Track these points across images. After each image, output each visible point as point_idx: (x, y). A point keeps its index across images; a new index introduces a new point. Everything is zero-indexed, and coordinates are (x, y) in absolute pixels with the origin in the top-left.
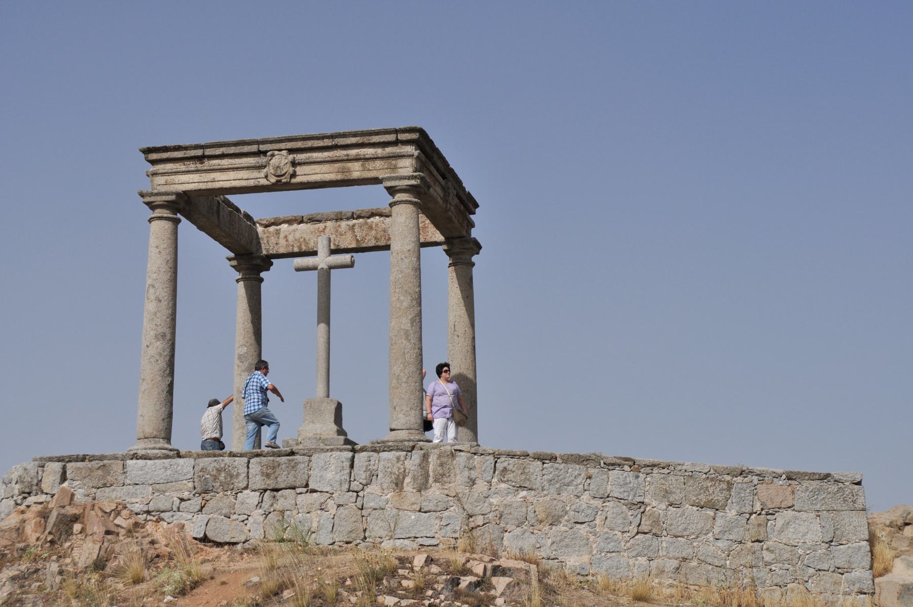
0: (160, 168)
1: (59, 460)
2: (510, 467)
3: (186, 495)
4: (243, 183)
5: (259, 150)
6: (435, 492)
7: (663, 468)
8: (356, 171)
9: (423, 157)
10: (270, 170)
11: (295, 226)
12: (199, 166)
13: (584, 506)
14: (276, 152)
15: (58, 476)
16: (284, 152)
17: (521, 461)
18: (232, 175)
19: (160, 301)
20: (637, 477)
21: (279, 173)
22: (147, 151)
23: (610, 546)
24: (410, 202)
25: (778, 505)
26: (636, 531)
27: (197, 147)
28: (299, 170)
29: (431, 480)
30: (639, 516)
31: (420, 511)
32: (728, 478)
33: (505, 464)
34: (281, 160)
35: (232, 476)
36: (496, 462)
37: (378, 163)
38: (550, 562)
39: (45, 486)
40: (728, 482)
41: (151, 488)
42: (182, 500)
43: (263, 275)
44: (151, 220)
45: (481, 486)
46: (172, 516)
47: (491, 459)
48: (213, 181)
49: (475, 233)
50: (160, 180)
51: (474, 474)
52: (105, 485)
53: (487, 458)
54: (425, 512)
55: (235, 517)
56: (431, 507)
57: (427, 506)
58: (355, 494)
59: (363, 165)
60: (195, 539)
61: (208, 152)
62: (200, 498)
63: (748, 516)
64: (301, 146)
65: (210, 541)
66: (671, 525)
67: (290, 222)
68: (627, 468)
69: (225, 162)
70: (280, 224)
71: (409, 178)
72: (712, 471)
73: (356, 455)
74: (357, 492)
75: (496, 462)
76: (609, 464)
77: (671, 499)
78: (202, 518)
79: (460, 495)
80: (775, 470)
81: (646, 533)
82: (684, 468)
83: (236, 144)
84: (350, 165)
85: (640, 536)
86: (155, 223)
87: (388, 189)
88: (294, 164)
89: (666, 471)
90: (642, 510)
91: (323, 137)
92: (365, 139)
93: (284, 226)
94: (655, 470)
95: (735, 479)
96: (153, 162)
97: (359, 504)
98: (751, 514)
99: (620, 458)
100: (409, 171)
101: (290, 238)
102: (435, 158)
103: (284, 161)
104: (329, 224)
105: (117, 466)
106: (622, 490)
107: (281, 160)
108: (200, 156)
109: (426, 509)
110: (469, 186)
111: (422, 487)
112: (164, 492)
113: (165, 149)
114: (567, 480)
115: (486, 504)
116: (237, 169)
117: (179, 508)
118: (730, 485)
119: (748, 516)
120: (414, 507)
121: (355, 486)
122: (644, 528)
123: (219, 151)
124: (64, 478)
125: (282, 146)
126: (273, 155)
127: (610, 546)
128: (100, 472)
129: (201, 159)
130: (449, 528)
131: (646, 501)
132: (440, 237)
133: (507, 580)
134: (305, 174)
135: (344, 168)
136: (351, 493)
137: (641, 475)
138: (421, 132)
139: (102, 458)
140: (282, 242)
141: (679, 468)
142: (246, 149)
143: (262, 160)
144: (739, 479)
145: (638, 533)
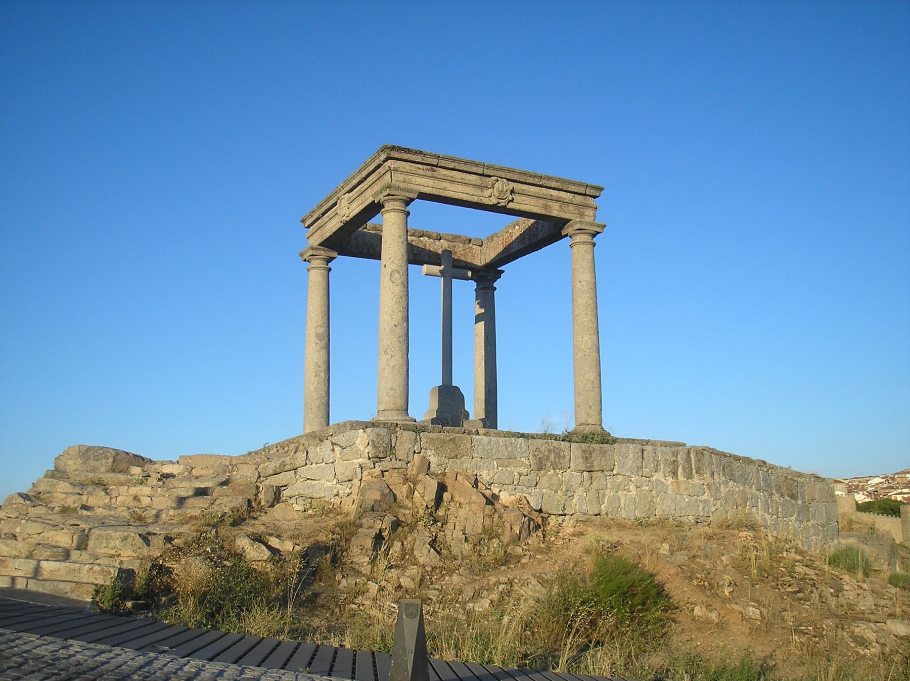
4: (469, 198)
6: (696, 480)
12: (429, 173)
18: (460, 188)
24: (583, 243)
28: (517, 198)
29: (694, 471)
35: (560, 457)
37: (571, 208)
42: (520, 475)
43: (440, 252)
48: (445, 189)
52: (456, 457)
59: (560, 206)
61: (442, 163)
83: (466, 163)
84: (550, 203)
113: (408, 151)
116: (365, 179)
123: (451, 165)
125: (503, 174)
128: (452, 445)
135: (546, 205)
142: (474, 169)
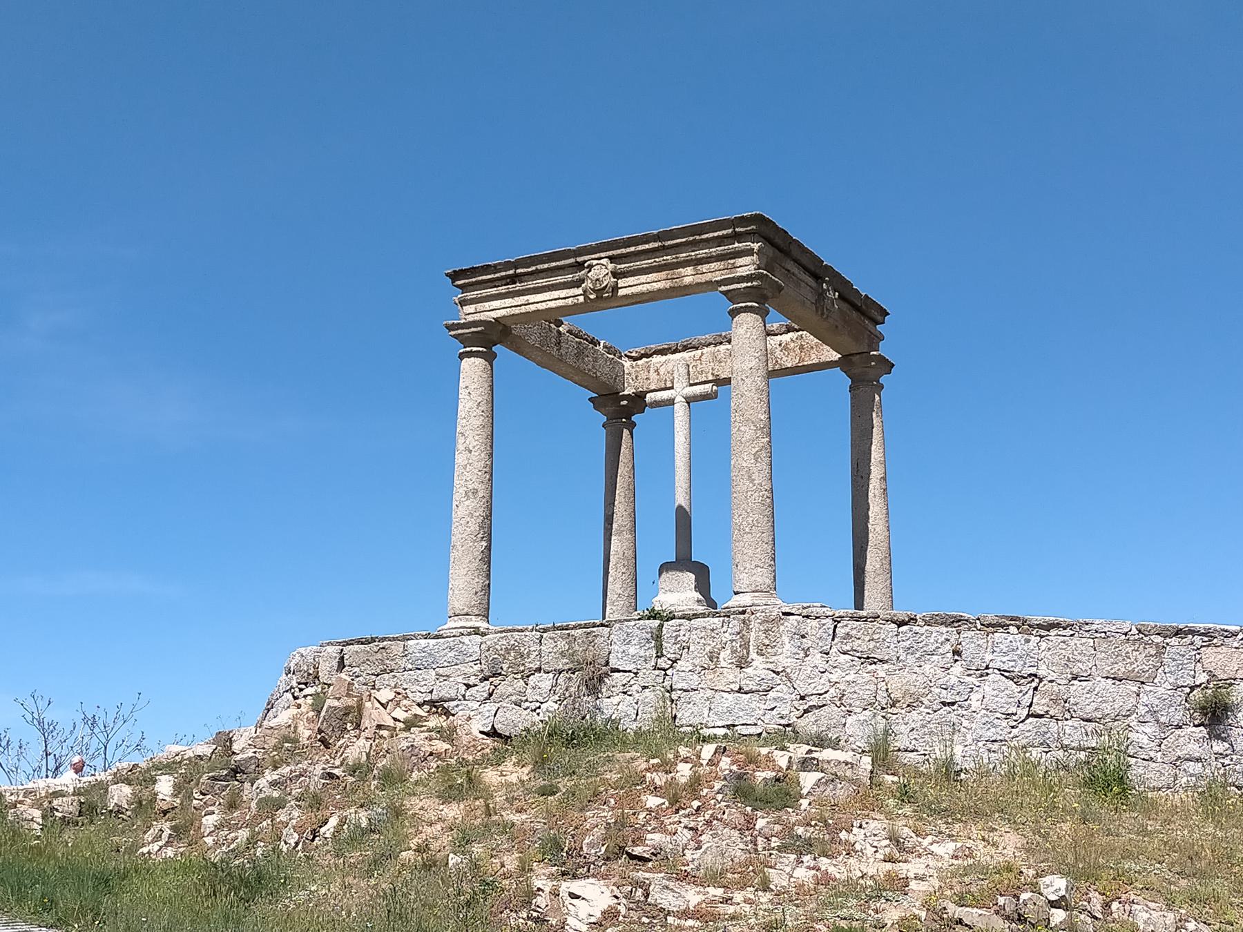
2: (853, 633)
3: (472, 681)
5: (569, 263)
7: (1065, 629)
8: (688, 276)
9: (770, 251)
10: (588, 284)
11: (670, 356)
13: (954, 680)
14: (595, 262)
15: (335, 663)
16: (604, 261)
19: (470, 452)
20: (1028, 641)
21: (598, 287)
22: (455, 276)
23: (989, 734)
25: (1232, 675)
27: (508, 265)
28: (621, 283)
30: (1031, 692)
32: (1158, 639)
38: (911, 754)
39: (323, 677)
41: (433, 673)
42: (468, 686)
44: (462, 356)
45: (816, 658)
50: (470, 309)
51: (807, 643)
54: (746, 693)
55: (527, 704)
60: (481, 732)
63: (1188, 690)
64: (625, 253)
65: (500, 736)
68: (1013, 629)
69: (541, 282)
71: (748, 278)
72: (1134, 631)
73: (666, 624)
78: (491, 707)
79: (788, 670)
80: (1226, 627)
81: (1041, 716)
82: (1094, 627)
85: (1031, 720)
86: (466, 363)
87: (725, 293)
88: (615, 274)
89: (1068, 632)
90: (1034, 685)
92: (695, 235)
93: (657, 359)
94: (1053, 632)
98: (1192, 688)
100: (751, 270)
101: (662, 371)
102: (795, 252)
103: (604, 271)
104: (706, 350)
105: (397, 648)
106: (1004, 659)
107: (601, 270)
108: (513, 275)
109: (746, 689)
110: (863, 287)
115: (822, 681)
117: (464, 696)
118: (1161, 649)
119: (1188, 690)
121: (662, 663)
122: (1037, 709)
124: (341, 665)
126: (590, 267)
127: (989, 734)
129: (513, 279)
130: (774, 712)
132: (836, 356)
133: (714, 746)
134: (630, 285)
136: (657, 672)
137: (1032, 638)
138: (759, 219)
140: (653, 375)
141: (1087, 627)
143: (577, 276)
144: (1174, 641)
145: (1028, 716)
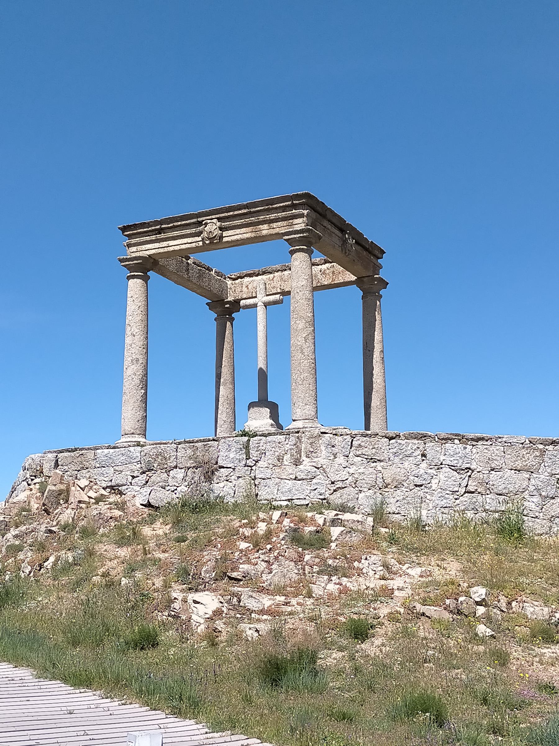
0: (133, 241)
1: (55, 452)
7: (487, 441)
8: (265, 230)
9: (314, 215)
10: (205, 234)
11: (254, 278)
15: (53, 464)
16: (215, 221)
17: (372, 439)
19: (134, 336)
22: (124, 229)
23: (442, 503)
26: (464, 490)
28: (225, 234)
30: (467, 478)
31: (295, 479)
32: (541, 447)
33: (359, 442)
34: (212, 227)
36: (352, 440)
40: (541, 450)
41: (113, 470)
42: (133, 477)
44: (129, 278)
45: (341, 460)
46: (127, 489)
47: (349, 438)
49: (382, 274)
53: (345, 437)
54: (299, 480)
56: (302, 476)
57: (301, 476)
58: (250, 468)
62: (145, 475)
65: (152, 506)
66: (493, 485)
67: (250, 275)
68: (457, 441)
70: (243, 277)
72: (528, 442)
74: (251, 467)
75: (352, 440)
76: (443, 439)
77: (493, 466)
79: (324, 467)
81: (473, 492)
82: (504, 439)
85: (466, 494)
86: (131, 282)
87: (287, 240)
89: (489, 443)
90: (469, 474)
91: (239, 208)
92: (269, 205)
93: (247, 279)
94: (480, 443)
95: (547, 447)
96: (130, 237)
97: (252, 475)
99: (451, 434)
100: (302, 226)
102: (329, 216)
103: (215, 227)
104: (276, 274)
106: (452, 459)
107: (212, 227)
108: (159, 229)
111: (297, 462)
112: (122, 471)
114: (409, 452)
115: (344, 473)
118: (542, 453)
120: (291, 476)
122: (471, 488)
124: (57, 465)
127: (442, 503)
129: (160, 231)
131: (472, 467)
132: (354, 278)
134: (230, 236)
136: (246, 468)
137: (468, 446)
139: (81, 449)
140: (245, 289)
141: (500, 440)
144: (550, 447)
145: (465, 492)
